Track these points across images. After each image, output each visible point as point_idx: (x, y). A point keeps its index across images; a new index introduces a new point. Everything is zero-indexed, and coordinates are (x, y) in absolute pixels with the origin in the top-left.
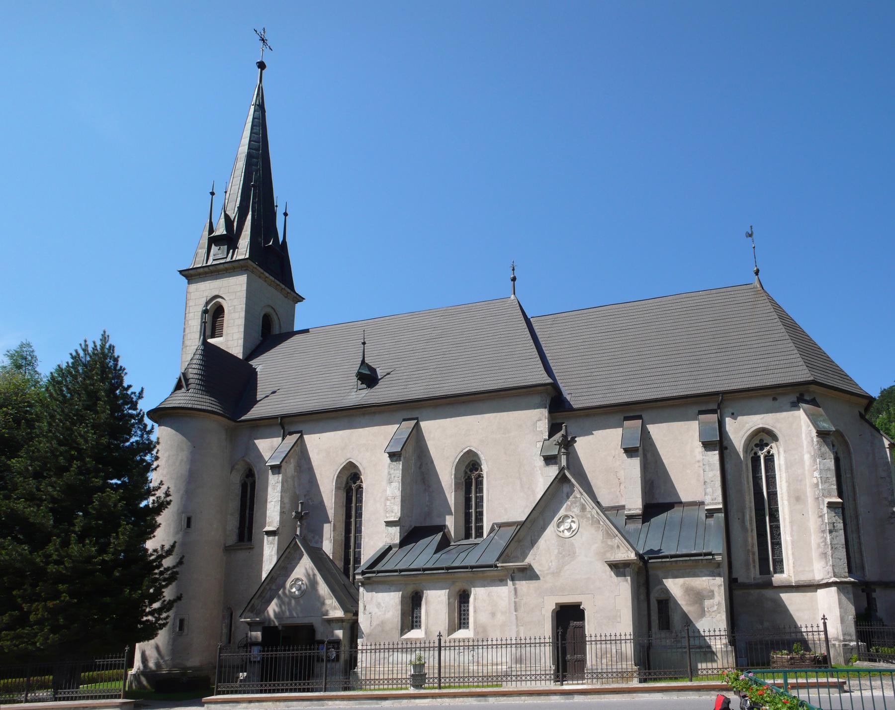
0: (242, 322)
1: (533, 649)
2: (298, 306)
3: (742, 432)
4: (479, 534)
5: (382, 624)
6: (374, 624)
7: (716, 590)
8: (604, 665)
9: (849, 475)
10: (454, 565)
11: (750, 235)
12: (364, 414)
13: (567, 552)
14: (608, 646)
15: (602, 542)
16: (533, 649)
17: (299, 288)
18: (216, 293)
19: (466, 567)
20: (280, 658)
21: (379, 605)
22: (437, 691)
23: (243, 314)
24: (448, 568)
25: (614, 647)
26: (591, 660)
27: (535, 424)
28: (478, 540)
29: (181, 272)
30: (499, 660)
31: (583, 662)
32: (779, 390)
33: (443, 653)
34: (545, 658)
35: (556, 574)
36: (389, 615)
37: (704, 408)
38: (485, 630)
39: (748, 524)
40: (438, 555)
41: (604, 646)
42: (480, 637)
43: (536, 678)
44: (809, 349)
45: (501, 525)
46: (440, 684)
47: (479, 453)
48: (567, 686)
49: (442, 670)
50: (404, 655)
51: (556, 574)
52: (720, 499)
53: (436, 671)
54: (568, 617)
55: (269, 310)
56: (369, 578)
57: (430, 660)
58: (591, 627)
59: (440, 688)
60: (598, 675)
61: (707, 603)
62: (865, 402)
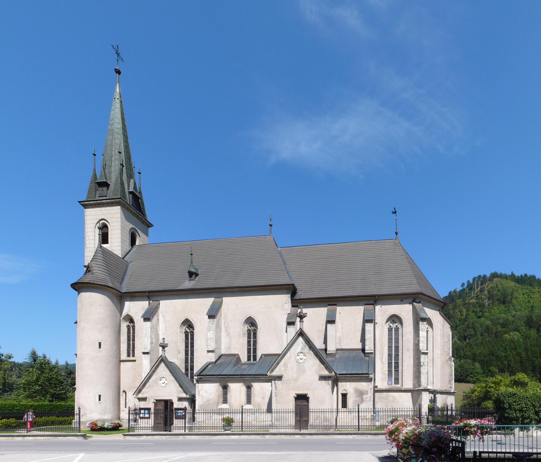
0: (87, 230)
1: (285, 414)
2: (150, 229)
3: (385, 315)
4: (255, 359)
5: (208, 400)
6: (204, 401)
7: (369, 390)
8: (317, 423)
9: (432, 340)
10: (244, 373)
11: (395, 213)
12: (193, 294)
13: (301, 370)
14: (318, 414)
15: (318, 366)
16: (285, 414)
17: (150, 217)
18: (101, 218)
19: (250, 375)
20: (481, 413)
21: (206, 392)
22: (241, 432)
23: (119, 231)
24: (241, 375)
25: (323, 415)
26: (311, 421)
27: (283, 306)
28: (255, 362)
29: (80, 202)
30: (267, 419)
31: (307, 421)
32: (404, 296)
33: (244, 415)
34: (291, 419)
35: (296, 380)
36: (211, 397)
37: (367, 303)
38: (259, 406)
39: (384, 360)
40: (236, 367)
41: (318, 414)
42: (257, 408)
43: (286, 427)
44: (420, 277)
45: (266, 355)
46: (242, 429)
47: (255, 318)
48: (303, 431)
49: (244, 424)
50: (350, 414)
51: (296, 380)
52: (373, 349)
53: (241, 424)
54: (302, 399)
55: (133, 230)
56: (201, 378)
57: (237, 418)
58: (313, 405)
59: (242, 431)
60: (314, 427)
61: (364, 396)
62: (443, 304)
